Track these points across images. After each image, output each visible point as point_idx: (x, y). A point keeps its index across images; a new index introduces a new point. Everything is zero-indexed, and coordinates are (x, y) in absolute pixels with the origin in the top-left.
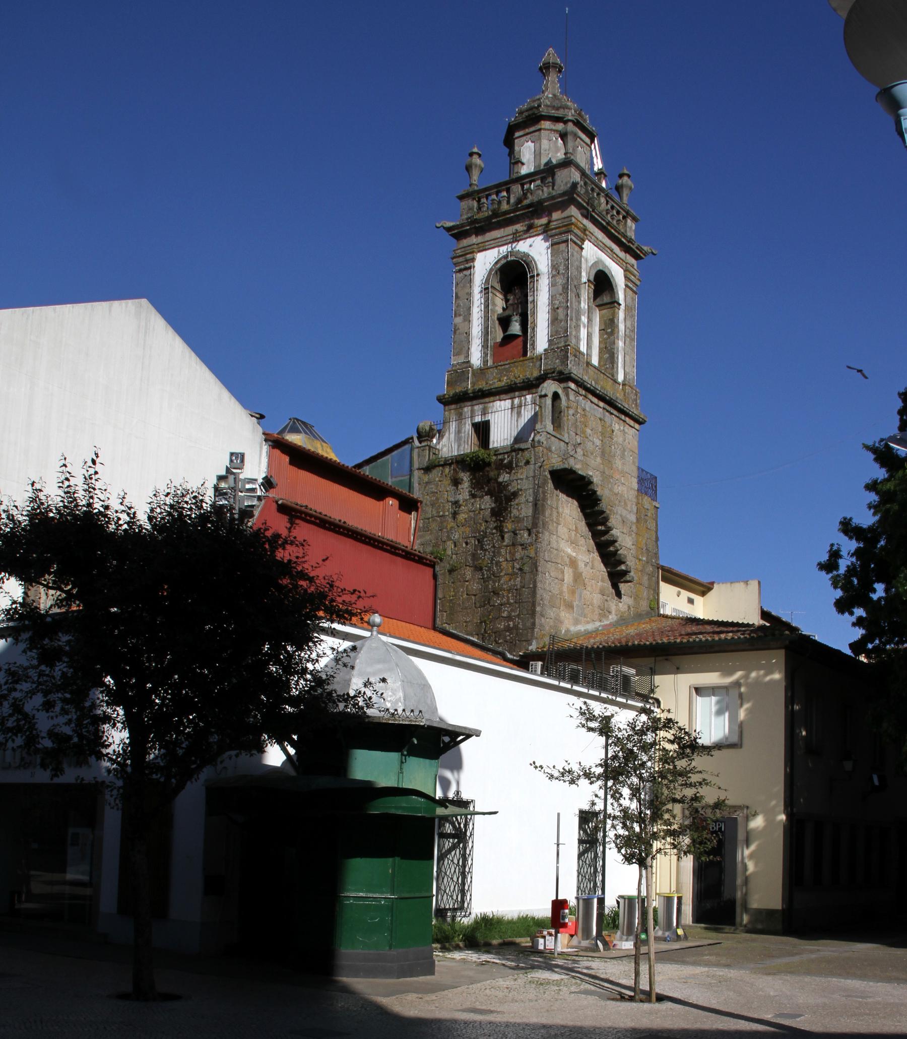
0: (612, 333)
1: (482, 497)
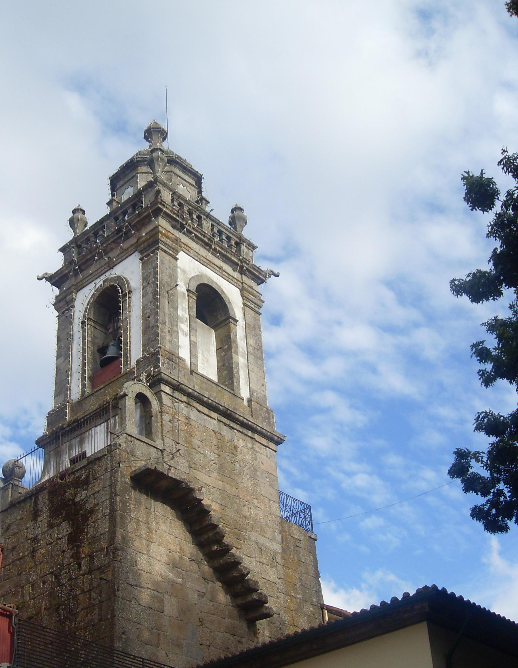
0: (230, 348)
1: (58, 525)
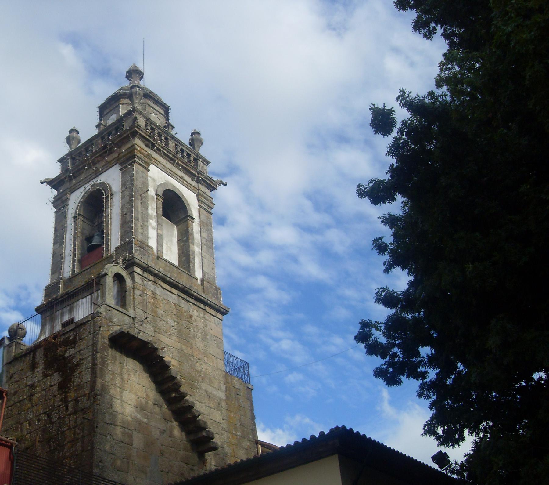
0: (188, 240)
1: (51, 375)
